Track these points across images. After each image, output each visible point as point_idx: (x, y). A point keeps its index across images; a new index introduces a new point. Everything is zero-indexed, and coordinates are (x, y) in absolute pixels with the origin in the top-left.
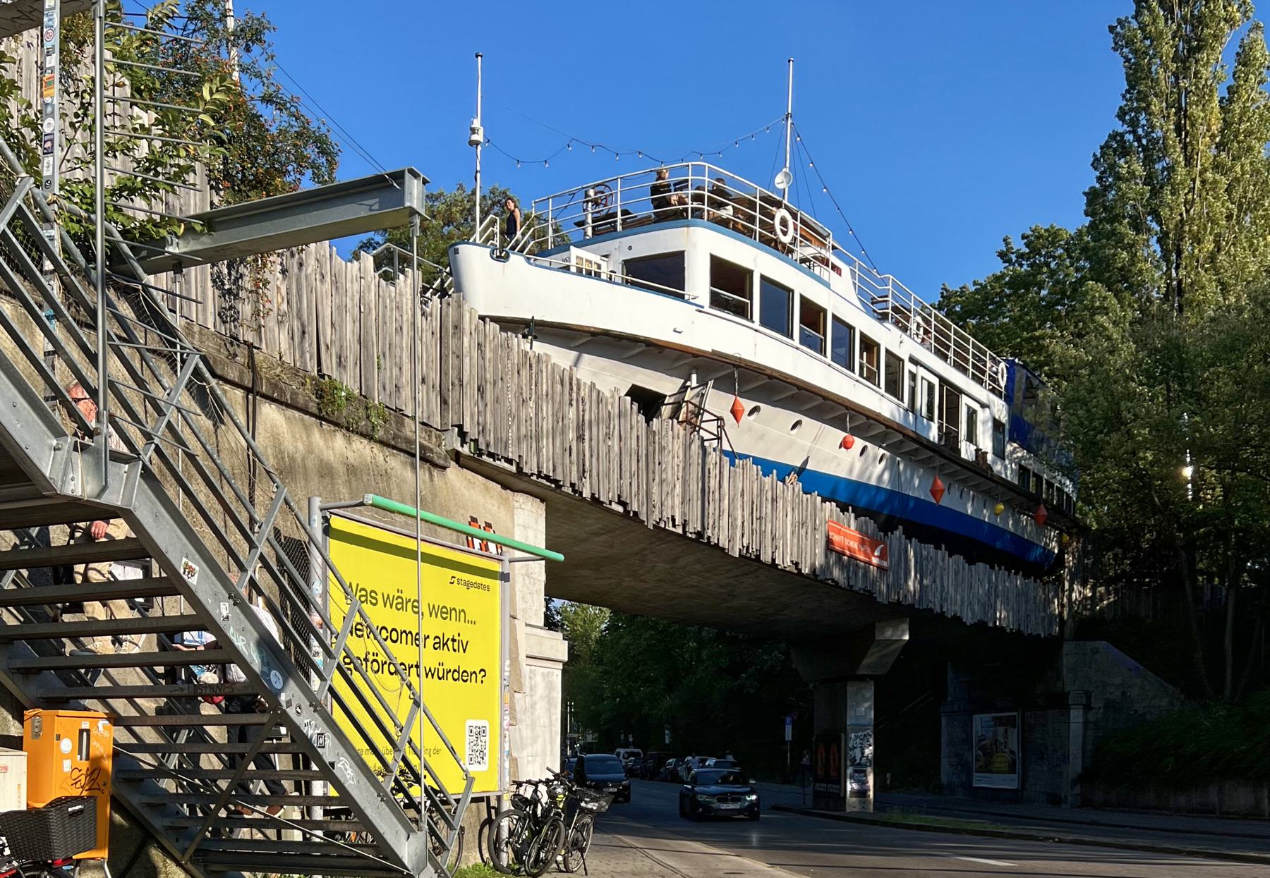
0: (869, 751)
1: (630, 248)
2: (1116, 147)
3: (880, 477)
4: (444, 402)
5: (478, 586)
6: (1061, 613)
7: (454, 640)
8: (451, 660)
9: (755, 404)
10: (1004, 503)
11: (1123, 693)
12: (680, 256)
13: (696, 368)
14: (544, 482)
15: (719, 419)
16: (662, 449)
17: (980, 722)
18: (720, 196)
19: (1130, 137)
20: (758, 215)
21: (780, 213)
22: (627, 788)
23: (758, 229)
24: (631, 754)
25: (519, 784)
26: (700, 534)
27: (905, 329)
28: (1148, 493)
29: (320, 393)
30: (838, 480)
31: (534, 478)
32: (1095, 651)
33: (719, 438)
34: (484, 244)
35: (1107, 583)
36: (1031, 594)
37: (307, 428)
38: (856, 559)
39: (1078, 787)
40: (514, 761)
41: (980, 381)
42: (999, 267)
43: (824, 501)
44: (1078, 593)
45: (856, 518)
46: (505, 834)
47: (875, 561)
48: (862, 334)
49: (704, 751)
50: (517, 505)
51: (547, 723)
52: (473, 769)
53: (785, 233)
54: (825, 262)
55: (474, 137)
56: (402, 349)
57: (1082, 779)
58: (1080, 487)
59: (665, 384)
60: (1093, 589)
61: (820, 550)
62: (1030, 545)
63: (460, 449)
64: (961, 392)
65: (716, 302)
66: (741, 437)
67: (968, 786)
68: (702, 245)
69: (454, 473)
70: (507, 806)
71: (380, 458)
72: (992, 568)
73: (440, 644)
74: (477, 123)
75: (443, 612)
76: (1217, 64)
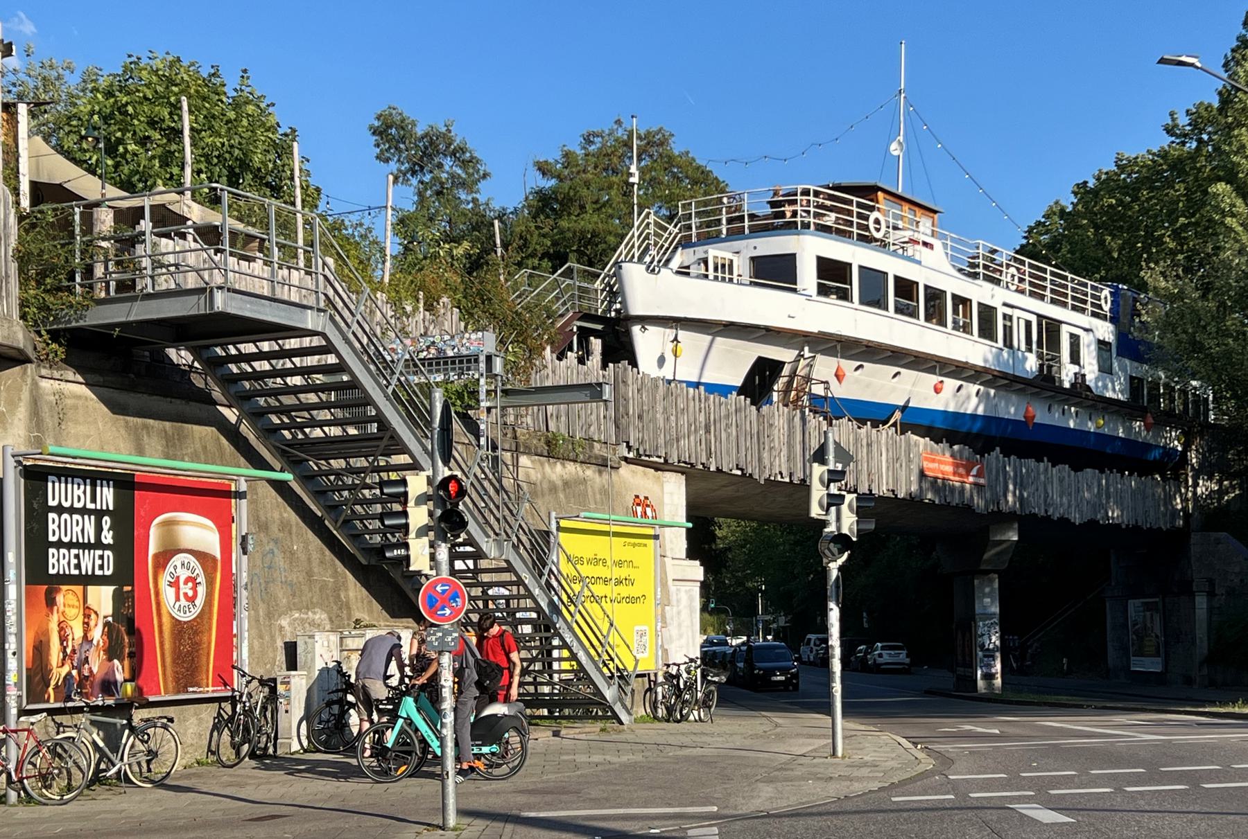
3: (976, 409)
5: (639, 545)
8: (624, 590)
9: (859, 363)
11: (1242, 581)
12: (794, 255)
13: (808, 343)
16: (771, 425)
17: (1134, 605)
22: (795, 676)
25: (668, 666)
29: (548, 443)
32: (1218, 542)
34: (640, 260)
35: (1230, 477)
37: (542, 464)
40: (665, 651)
42: (1165, 141)
44: (1204, 487)
46: (660, 697)
52: (638, 657)
59: (784, 355)
60: (1220, 482)
61: (914, 478)
62: (1147, 447)
65: (823, 291)
68: (809, 249)
69: (626, 471)
70: (661, 679)
71: (581, 473)
72: (1102, 472)
73: (619, 582)
74: (633, 169)
75: (619, 564)
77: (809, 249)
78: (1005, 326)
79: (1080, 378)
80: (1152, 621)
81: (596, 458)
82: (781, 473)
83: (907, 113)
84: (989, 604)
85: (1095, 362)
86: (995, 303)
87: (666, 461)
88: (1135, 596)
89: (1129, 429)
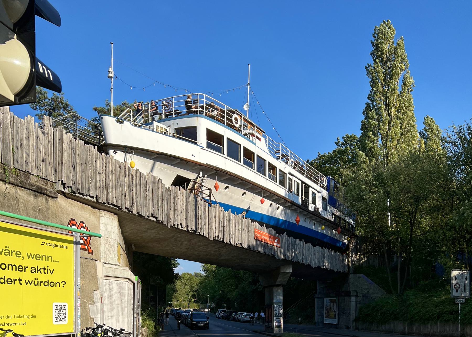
0: (281, 311)
1: (177, 124)
2: (368, 108)
4: (55, 170)
6: (348, 264)
7: (44, 269)
9: (227, 185)
10: (325, 226)
11: (368, 292)
12: (196, 127)
13: (202, 170)
14: (112, 206)
15: (209, 189)
17: (326, 300)
18: (210, 107)
19: (372, 105)
20: (225, 115)
21: (235, 116)
22: (207, 324)
23: (226, 121)
24: (223, 311)
26: (195, 231)
27: (287, 163)
28: (375, 226)
30: (263, 215)
31: (107, 204)
32: (359, 277)
33: (210, 196)
36: (337, 258)
38: (267, 243)
39: (354, 323)
41: (317, 184)
42: (336, 147)
43: (253, 221)
44: (355, 257)
45: (267, 229)
47: (275, 244)
48: (269, 163)
49: (243, 310)
50: (101, 215)
51: (119, 303)
53: (237, 123)
54: (253, 135)
55: (110, 75)
56: (29, 146)
57: (356, 320)
58: (356, 221)
59: (191, 176)
60: (360, 256)
62: (337, 241)
63: (63, 190)
64: (310, 187)
65: (209, 146)
66: (218, 196)
67: (323, 322)
68: (203, 125)
69: (61, 200)
71: (14, 190)
72: (322, 248)
73: (35, 270)
74: (111, 69)
76: (397, 84)
77: (203, 125)
78: (289, 183)
79: (316, 209)
80: (333, 306)
81: (30, 184)
82: (181, 224)
83: (250, 94)
84: (279, 297)
85: (321, 204)
86: (286, 171)
87: (97, 200)
88: (327, 297)
89: (331, 233)
